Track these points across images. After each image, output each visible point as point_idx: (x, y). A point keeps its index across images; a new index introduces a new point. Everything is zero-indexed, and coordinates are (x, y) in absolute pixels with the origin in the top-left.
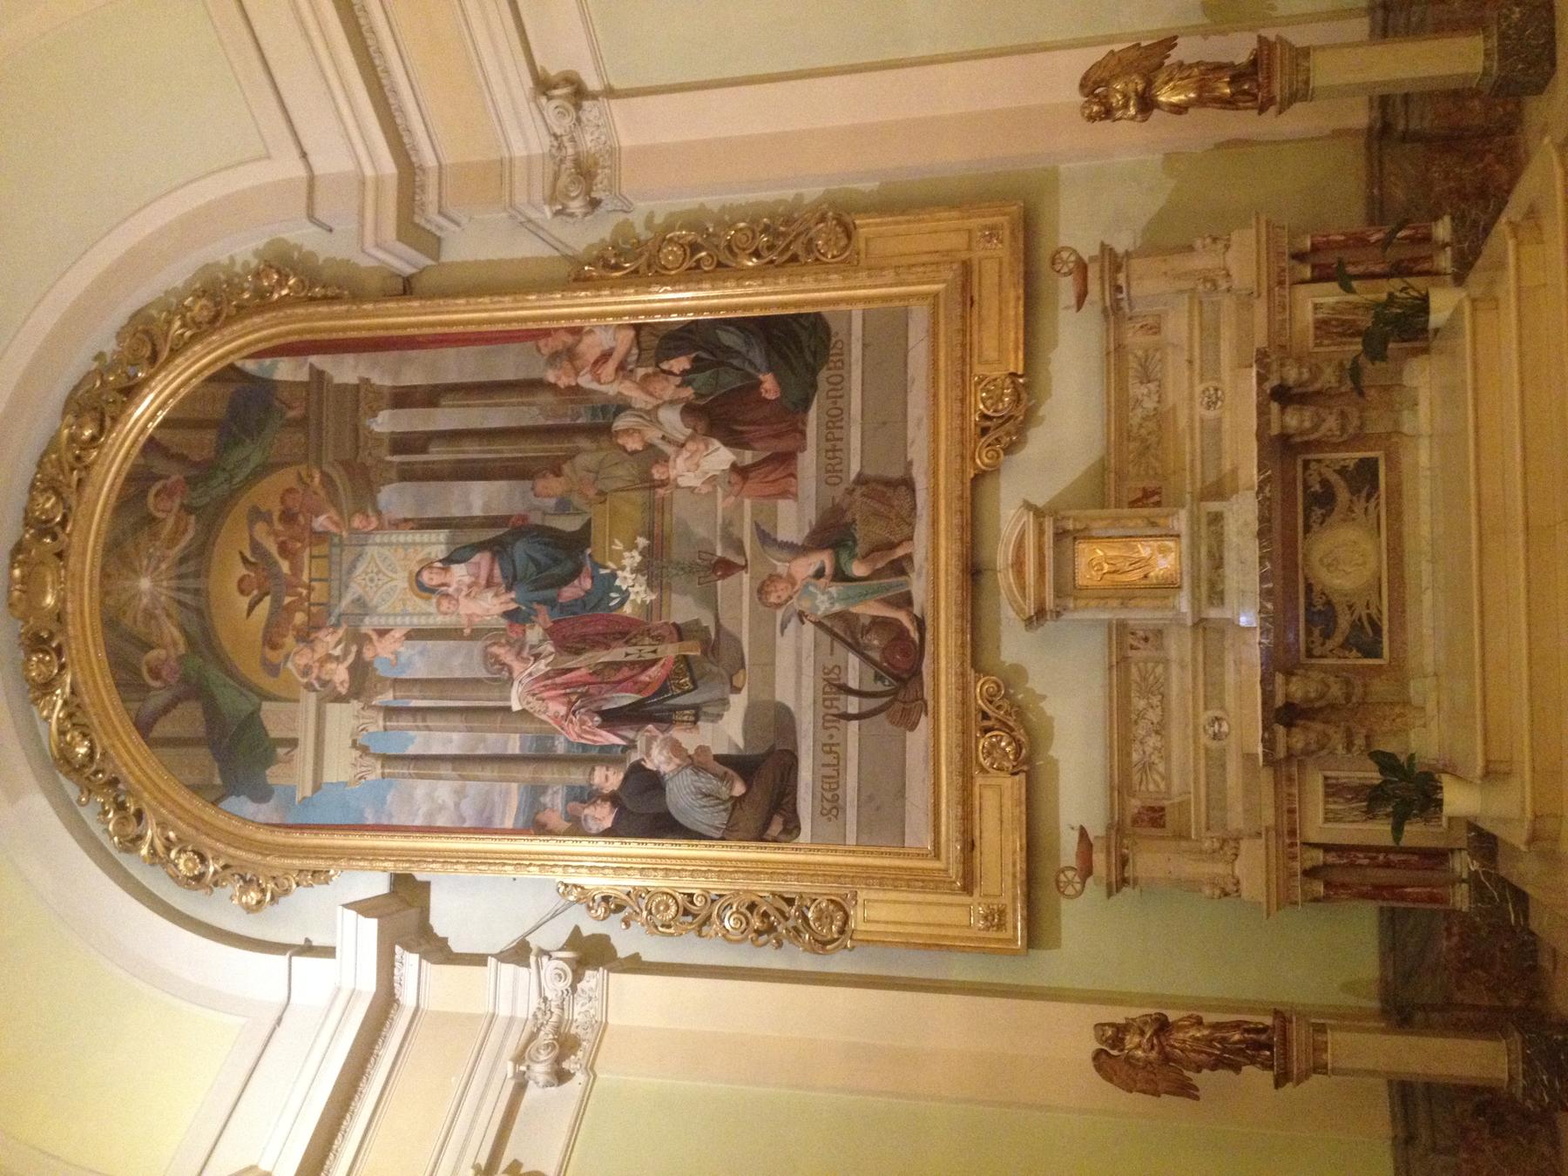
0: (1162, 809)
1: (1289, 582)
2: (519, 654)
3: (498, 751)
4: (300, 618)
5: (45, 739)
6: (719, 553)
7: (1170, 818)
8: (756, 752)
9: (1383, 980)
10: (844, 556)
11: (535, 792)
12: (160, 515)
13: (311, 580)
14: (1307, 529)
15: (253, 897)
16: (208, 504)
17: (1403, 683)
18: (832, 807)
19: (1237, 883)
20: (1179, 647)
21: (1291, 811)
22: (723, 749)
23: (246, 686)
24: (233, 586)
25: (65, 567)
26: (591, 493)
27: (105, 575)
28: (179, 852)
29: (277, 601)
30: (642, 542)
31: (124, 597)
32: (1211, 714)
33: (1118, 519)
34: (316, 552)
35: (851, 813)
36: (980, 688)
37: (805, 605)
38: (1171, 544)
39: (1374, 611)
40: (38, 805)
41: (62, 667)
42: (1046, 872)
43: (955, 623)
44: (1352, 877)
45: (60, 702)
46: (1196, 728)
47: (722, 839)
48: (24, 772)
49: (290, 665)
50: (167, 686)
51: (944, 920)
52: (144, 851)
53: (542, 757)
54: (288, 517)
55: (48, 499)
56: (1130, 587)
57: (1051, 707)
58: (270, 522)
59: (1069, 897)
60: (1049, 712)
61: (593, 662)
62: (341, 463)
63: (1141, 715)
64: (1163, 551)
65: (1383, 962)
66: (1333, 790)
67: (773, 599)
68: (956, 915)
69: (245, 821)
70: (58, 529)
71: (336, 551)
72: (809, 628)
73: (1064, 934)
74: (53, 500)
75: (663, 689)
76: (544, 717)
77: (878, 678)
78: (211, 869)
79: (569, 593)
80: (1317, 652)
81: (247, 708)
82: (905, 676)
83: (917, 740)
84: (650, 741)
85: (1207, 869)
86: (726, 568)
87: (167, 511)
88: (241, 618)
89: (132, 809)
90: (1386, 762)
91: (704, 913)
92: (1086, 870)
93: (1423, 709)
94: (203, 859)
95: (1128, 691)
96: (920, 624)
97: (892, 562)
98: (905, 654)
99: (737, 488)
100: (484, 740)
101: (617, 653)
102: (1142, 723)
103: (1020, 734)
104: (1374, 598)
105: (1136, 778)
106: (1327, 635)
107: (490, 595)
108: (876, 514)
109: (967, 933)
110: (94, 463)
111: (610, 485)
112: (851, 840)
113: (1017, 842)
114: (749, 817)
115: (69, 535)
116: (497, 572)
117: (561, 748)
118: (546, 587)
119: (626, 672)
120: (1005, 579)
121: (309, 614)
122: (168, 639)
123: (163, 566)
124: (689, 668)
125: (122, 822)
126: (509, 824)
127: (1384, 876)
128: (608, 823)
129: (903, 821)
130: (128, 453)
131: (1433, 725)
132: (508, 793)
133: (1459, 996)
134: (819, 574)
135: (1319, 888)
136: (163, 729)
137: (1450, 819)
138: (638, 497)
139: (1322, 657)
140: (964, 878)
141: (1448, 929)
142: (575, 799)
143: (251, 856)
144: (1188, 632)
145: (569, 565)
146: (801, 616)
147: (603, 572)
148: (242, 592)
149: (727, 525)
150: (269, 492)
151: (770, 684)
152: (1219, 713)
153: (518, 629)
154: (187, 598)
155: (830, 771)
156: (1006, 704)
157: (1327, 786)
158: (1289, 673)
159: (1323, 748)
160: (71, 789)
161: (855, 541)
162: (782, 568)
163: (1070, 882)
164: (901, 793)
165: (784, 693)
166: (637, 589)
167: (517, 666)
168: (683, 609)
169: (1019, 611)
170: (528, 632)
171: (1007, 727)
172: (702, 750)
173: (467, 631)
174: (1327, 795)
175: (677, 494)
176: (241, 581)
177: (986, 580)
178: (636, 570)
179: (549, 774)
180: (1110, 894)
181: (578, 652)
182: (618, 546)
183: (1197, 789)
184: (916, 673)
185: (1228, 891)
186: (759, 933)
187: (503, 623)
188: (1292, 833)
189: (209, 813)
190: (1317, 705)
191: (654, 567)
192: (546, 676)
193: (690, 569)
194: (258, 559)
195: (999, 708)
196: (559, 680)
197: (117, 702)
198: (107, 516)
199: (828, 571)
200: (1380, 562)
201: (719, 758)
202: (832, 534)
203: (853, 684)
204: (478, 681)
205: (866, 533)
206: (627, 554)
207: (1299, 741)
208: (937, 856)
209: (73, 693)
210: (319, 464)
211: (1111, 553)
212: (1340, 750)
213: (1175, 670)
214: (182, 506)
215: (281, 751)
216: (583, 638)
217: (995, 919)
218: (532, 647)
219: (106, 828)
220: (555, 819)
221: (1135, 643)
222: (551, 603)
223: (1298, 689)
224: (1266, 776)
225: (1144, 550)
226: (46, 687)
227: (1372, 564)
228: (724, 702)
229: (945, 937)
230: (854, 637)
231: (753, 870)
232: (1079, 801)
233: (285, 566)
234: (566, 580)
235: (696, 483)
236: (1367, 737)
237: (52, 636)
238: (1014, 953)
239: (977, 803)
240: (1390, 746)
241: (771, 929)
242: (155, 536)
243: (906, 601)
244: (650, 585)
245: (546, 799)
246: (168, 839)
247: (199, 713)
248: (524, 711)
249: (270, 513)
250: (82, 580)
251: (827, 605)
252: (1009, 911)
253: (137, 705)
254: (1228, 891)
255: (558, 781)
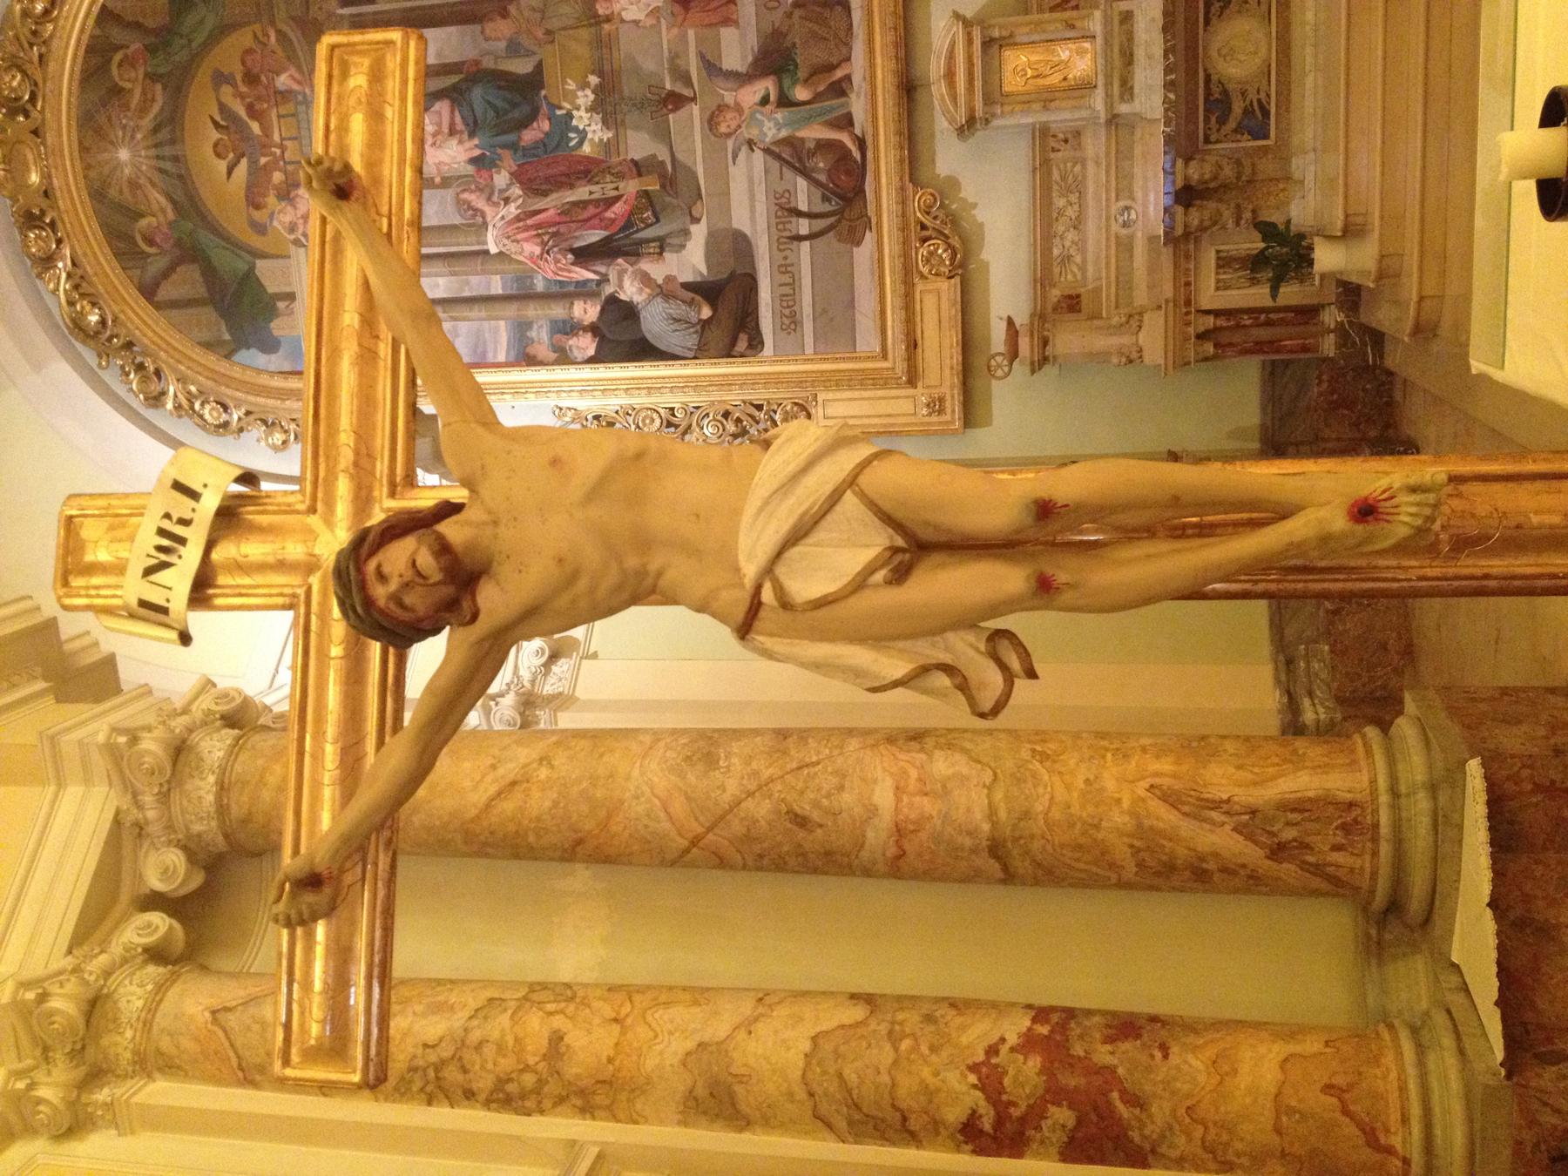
0: (1078, 296)
1: (1191, 72)
2: (489, 199)
3: (483, 292)
4: (277, 177)
5: (56, 311)
6: (668, 86)
7: (1084, 301)
8: (719, 277)
9: (1263, 426)
10: (787, 82)
11: (521, 329)
12: (128, 85)
13: (282, 139)
14: (1207, 22)
15: (278, 438)
16: (170, 73)
17: (1286, 161)
18: (790, 321)
19: (1141, 350)
20: (1095, 145)
21: (1188, 284)
22: (688, 277)
23: (236, 246)
24: (209, 151)
25: (44, 144)
26: (540, 34)
27: (84, 149)
28: (202, 404)
29: (253, 163)
30: (594, 80)
31: (106, 170)
32: (1122, 204)
33: (1039, 23)
34: (283, 111)
35: (808, 326)
36: (918, 200)
37: (754, 133)
38: (1087, 45)
39: (1263, 95)
40: (62, 370)
41: (59, 242)
42: (979, 361)
43: (894, 139)
44: (1237, 338)
45: (64, 276)
46: (1108, 219)
47: (695, 358)
48: (41, 340)
49: (275, 223)
50: (163, 253)
51: (890, 411)
52: (170, 406)
53: (524, 295)
54: (251, 78)
55: (14, 77)
56: (1051, 90)
57: (980, 215)
58: (235, 86)
59: (1000, 378)
60: (980, 219)
61: (559, 203)
62: (293, 18)
63: (1061, 213)
64: (1081, 53)
65: (1263, 409)
66: (1224, 262)
67: (723, 129)
68: (905, 406)
69: (259, 371)
70: (29, 107)
71: (302, 108)
72: (758, 156)
73: (995, 412)
74: (19, 77)
75: (628, 225)
76: (521, 258)
77: (825, 199)
78: (235, 417)
79: (529, 136)
80: (1213, 138)
81: (242, 267)
82: (850, 195)
83: (863, 254)
84: (621, 274)
85: (1114, 341)
86: (676, 101)
87: (132, 80)
88: (222, 181)
89: (152, 369)
90: (1268, 231)
91: (684, 424)
92: (1013, 354)
93: (1302, 182)
94: (225, 408)
95: (1050, 189)
96: (861, 143)
97: (833, 83)
98: (848, 173)
99: (680, 18)
100: (468, 283)
101: (582, 192)
102: (1062, 219)
103: (955, 241)
104: (1265, 82)
105: (1056, 270)
106: (1222, 121)
107: (454, 142)
108: (814, 35)
109: (912, 419)
110: (52, 36)
111: (554, 24)
112: (809, 350)
113: (953, 338)
114: (717, 336)
115: (42, 112)
116: (458, 119)
117: (540, 286)
118: (504, 132)
119: (591, 210)
120: (939, 90)
121: (285, 173)
122: (155, 207)
123: (139, 136)
124: (652, 205)
125: (144, 380)
126: (502, 358)
127: (1264, 334)
128: (591, 352)
129: (853, 329)
130: (84, 24)
131: (1311, 197)
132: (496, 331)
133: (1327, 433)
134: (765, 101)
135: (1209, 348)
136: (166, 292)
137: (1323, 276)
138: (585, 34)
139: (1217, 142)
140: (909, 371)
141: (1319, 377)
142: (559, 332)
143: (271, 402)
144: (1103, 131)
145: (526, 109)
146: (751, 144)
147: (559, 112)
148: (218, 155)
149: (674, 57)
150: (229, 54)
151: (726, 210)
152: (1128, 203)
153: (485, 174)
154: (168, 166)
155: (787, 290)
156: (941, 215)
157: (1218, 258)
158: (1188, 160)
159: (1215, 223)
160: (90, 357)
161: (796, 66)
162: (729, 98)
163: (999, 366)
164: (851, 304)
165: (740, 220)
166: (594, 127)
167: (488, 210)
168: (640, 145)
169: (951, 121)
170: (496, 177)
171: (945, 236)
172: (670, 279)
173: (438, 180)
174: (1219, 267)
175: (623, 29)
176: (216, 145)
177: (920, 96)
178: (591, 109)
179: (532, 311)
180: (1033, 372)
181: (545, 194)
182: (571, 85)
183: (1108, 273)
184: (861, 191)
185: (1132, 359)
186: (735, 436)
187: (470, 169)
188: (1188, 303)
189: (222, 366)
190: (1212, 185)
191: (606, 105)
192: (518, 219)
193: (640, 105)
194: (228, 123)
195: (935, 218)
196: (529, 222)
197: (119, 270)
198: (75, 89)
199: (772, 98)
200: (1270, 50)
201: (687, 286)
202: (774, 60)
203: (803, 207)
204: (454, 227)
205: (807, 57)
206: (580, 93)
207: (1195, 217)
208: (885, 357)
209: (74, 264)
210: (273, 23)
211: (1034, 58)
212: (1230, 225)
213: (1091, 169)
214: (147, 75)
215: (281, 305)
216: (547, 179)
217: (937, 405)
218: (501, 191)
219: (131, 389)
220: (543, 350)
221: (1056, 146)
222: (514, 147)
223: (1195, 172)
224: (1166, 254)
225: (1063, 53)
226: (47, 262)
227: (1263, 51)
228: (686, 233)
229: (893, 425)
230: (800, 160)
231: (726, 383)
232: (1006, 295)
233: (255, 127)
234: (525, 123)
235: (641, 16)
236: (1254, 211)
237: (43, 213)
238: (954, 432)
239: (918, 307)
240: (1276, 218)
241: (744, 432)
242: (126, 107)
243: (846, 122)
244: (605, 122)
245: (533, 334)
246: (189, 393)
247: (197, 275)
248: (501, 253)
249: (232, 75)
250: (62, 156)
251: (774, 131)
252: (948, 398)
253: (138, 272)
254: (1132, 359)
255: (541, 318)
